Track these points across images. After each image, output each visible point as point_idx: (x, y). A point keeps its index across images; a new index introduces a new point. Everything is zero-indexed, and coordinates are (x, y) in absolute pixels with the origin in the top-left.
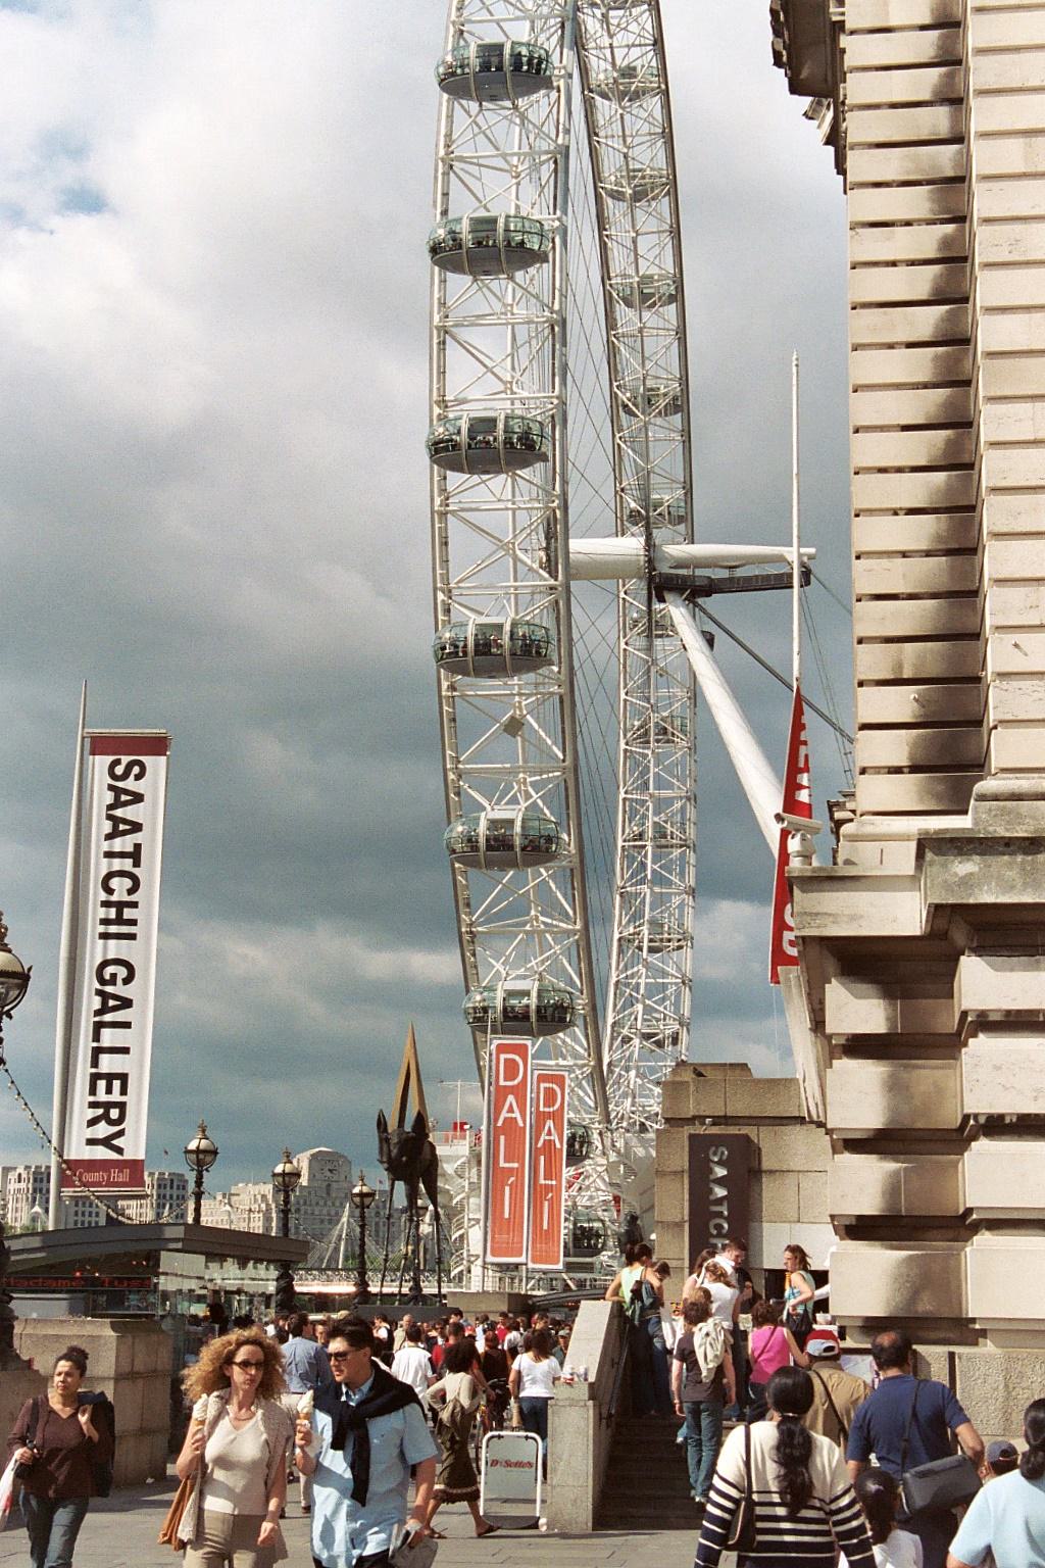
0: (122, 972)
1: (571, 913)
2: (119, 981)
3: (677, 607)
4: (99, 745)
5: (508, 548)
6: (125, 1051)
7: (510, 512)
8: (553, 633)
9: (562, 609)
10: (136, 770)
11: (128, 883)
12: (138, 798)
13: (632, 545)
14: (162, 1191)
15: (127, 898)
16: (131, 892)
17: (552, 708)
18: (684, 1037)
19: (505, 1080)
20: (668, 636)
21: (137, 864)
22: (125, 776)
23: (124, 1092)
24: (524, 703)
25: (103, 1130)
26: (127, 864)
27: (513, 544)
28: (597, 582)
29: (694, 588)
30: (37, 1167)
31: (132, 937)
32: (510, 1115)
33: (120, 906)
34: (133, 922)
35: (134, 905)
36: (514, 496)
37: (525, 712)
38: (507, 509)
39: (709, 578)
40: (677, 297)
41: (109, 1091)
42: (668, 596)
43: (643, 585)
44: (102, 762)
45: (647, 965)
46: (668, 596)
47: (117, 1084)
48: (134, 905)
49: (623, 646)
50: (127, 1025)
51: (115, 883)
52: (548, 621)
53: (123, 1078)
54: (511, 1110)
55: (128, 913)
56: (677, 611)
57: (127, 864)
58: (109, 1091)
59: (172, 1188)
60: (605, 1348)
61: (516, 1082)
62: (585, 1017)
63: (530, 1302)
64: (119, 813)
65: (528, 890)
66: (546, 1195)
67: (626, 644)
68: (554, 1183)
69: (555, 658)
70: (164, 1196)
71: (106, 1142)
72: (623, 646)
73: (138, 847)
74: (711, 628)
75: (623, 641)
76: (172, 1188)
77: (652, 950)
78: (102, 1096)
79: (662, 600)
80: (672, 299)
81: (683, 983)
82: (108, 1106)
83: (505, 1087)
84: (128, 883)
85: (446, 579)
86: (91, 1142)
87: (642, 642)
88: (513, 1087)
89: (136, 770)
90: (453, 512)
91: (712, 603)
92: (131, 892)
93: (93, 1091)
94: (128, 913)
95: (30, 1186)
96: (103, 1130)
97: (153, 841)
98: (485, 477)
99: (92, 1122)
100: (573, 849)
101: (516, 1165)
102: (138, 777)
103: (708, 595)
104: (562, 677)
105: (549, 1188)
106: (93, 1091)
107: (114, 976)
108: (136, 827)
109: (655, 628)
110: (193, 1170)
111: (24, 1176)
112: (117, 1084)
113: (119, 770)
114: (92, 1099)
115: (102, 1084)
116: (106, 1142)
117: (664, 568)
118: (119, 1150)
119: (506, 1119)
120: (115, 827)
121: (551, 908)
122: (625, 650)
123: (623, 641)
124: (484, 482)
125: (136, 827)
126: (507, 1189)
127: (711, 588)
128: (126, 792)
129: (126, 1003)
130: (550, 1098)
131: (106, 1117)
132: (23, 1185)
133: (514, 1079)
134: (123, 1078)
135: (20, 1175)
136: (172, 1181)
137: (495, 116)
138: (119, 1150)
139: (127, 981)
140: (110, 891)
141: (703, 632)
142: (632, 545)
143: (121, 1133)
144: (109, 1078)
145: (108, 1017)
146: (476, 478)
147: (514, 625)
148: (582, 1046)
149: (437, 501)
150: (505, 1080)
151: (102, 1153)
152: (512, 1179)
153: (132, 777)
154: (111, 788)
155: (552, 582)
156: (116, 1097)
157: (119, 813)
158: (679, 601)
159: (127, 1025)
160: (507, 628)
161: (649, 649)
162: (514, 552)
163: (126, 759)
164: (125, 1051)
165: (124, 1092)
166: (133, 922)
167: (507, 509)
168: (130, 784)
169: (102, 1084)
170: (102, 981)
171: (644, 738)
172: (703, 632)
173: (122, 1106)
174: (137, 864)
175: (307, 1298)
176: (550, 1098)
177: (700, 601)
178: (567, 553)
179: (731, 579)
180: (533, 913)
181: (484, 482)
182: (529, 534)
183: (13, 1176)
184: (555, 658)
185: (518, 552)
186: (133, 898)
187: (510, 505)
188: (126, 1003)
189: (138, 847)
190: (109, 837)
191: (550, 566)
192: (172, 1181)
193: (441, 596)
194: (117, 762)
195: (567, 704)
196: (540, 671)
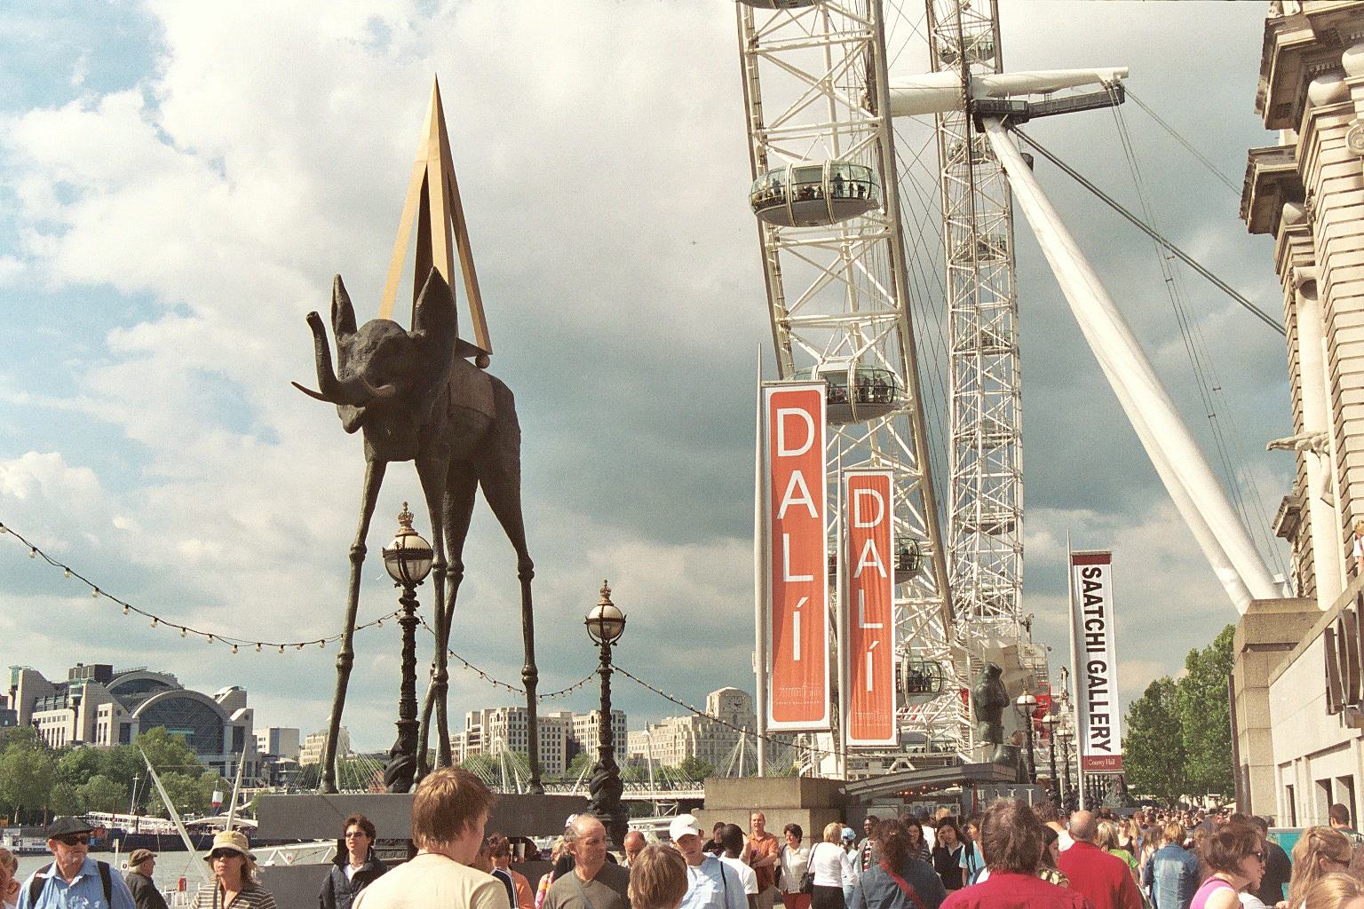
0: (1100, 667)
1: (913, 460)
2: (1100, 671)
3: (996, 132)
4: (1078, 559)
5: (827, 88)
6: (1106, 703)
7: (824, 47)
8: (876, 173)
9: (885, 146)
10: (1097, 573)
11: (1098, 625)
12: (1099, 586)
13: (950, 78)
14: (513, 722)
15: (1098, 632)
16: (1100, 629)
20: (984, 162)
21: (1101, 616)
22: (1091, 576)
23: (1107, 722)
24: (850, 248)
25: (1100, 740)
26: (1096, 616)
27: (830, 82)
28: (915, 117)
29: (1012, 118)
30: (511, 709)
31: (1103, 650)
32: (870, 564)
33: (1096, 636)
34: (1103, 643)
35: (1102, 635)
36: (827, 31)
37: (853, 257)
38: (819, 44)
39: (1026, 102)
41: (1100, 722)
42: (987, 124)
43: (963, 115)
44: (1081, 568)
46: (987, 124)
47: (1104, 719)
48: (1102, 635)
49: (944, 174)
50: (1105, 691)
51: (1091, 625)
52: (869, 160)
53: (1107, 716)
54: (797, 493)
55: (1100, 639)
56: (997, 139)
57: (1096, 616)
58: (1100, 722)
59: (520, 720)
62: (932, 559)
63: (842, 791)
64: (1088, 593)
65: (868, 438)
67: (947, 172)
68: (880, 626)
69: (880, 201)
70: (515, 726)
71: (1102, 746)
72: (944, 174)
73: (1101, 608)
75: (943, 171)
76: (520, 720)
78: (1097, 724)
81: (1016, 515)
82: (1100, 729)
84: (1098, 625)
85: (760, 126)
86: (1094, 746)
87: (962, 168)
89: (1097, 573)
90: (763, 53)
91: (1031, 127)
92: (1100, 629)
93: (1092, 723)
94: (1100, 639)
95: (506, 723)
96: (1100, 740)
97: (1108, 605)
98: (795, 12)
99: (1094, 736)
100: (910, 396)
101: (809, 578)
102: (1098, 576)
104: (890, 220)
106: (1092, 723)
107: (1096, 669)
108: (1100, 600)
109: (974, 155)
111: (502, 715)
112: (1104, 719)
113: (1088, 573)
114: (1092, 726)
115: (1096, 720)
116: (1102, 746)
117: (981, 96)
118: (1109, 750)
120: (1089, 600)
121: (890, 449)
122: (946, 178)
123: (943, 171)
124: (794, 19)
125: (1100, 600)
127: (1027, 114)
128: (1093, 583)
129: (1104, 681)
131: (1100, 734)
132: (501, 723)
134: (1107, 716)
135: (593, 717)
136: (520, 714)
138: (1109, 750)
139: (1103, 671)
140: (1091, 629)
141: (1022, 154)
142: (950, 78)
143: (1108, 742)
144: (1100, 716)
145: (1094, 688)
146: (785, 15)
148: (931, 583)
149: (746, 43)
151: (1103, 752)
152: (804, 600)
153: (1090, 570)
154: (1084, 582)
155: (871, 118)
156: (1104, 725)
157: (1088, 593)
158: (998, 126)
159: (1105, 691)
161: (970, 176)
162: (831, 90)
163: (1091, 567)
164: (1106, 703)
165: (1107, 722)
166: (1103, 643)
167: (819, 44)
168: (1094, 579)
169: (1096, 720)
170: (1091, 671)
172: (1022, 154)
173: (1107, 729)
174: (1101, 616)
178: (886, 88)
179: (1046, 103)
180: (873, 455)
181: (794, 19)
182: (845, 70)
183: (493, 716)
184: (880, 201)
185: (835, 90)
186: (1101, 632)
187: (822, 40)
188: (1104, 681)
189: (1101, 608)
190: (1086, 605)
191: (871, 101)
192: (520, 714)
193: (756, 143)
194: (1087, 569)
195: (896, 242)
196: (865, 214)
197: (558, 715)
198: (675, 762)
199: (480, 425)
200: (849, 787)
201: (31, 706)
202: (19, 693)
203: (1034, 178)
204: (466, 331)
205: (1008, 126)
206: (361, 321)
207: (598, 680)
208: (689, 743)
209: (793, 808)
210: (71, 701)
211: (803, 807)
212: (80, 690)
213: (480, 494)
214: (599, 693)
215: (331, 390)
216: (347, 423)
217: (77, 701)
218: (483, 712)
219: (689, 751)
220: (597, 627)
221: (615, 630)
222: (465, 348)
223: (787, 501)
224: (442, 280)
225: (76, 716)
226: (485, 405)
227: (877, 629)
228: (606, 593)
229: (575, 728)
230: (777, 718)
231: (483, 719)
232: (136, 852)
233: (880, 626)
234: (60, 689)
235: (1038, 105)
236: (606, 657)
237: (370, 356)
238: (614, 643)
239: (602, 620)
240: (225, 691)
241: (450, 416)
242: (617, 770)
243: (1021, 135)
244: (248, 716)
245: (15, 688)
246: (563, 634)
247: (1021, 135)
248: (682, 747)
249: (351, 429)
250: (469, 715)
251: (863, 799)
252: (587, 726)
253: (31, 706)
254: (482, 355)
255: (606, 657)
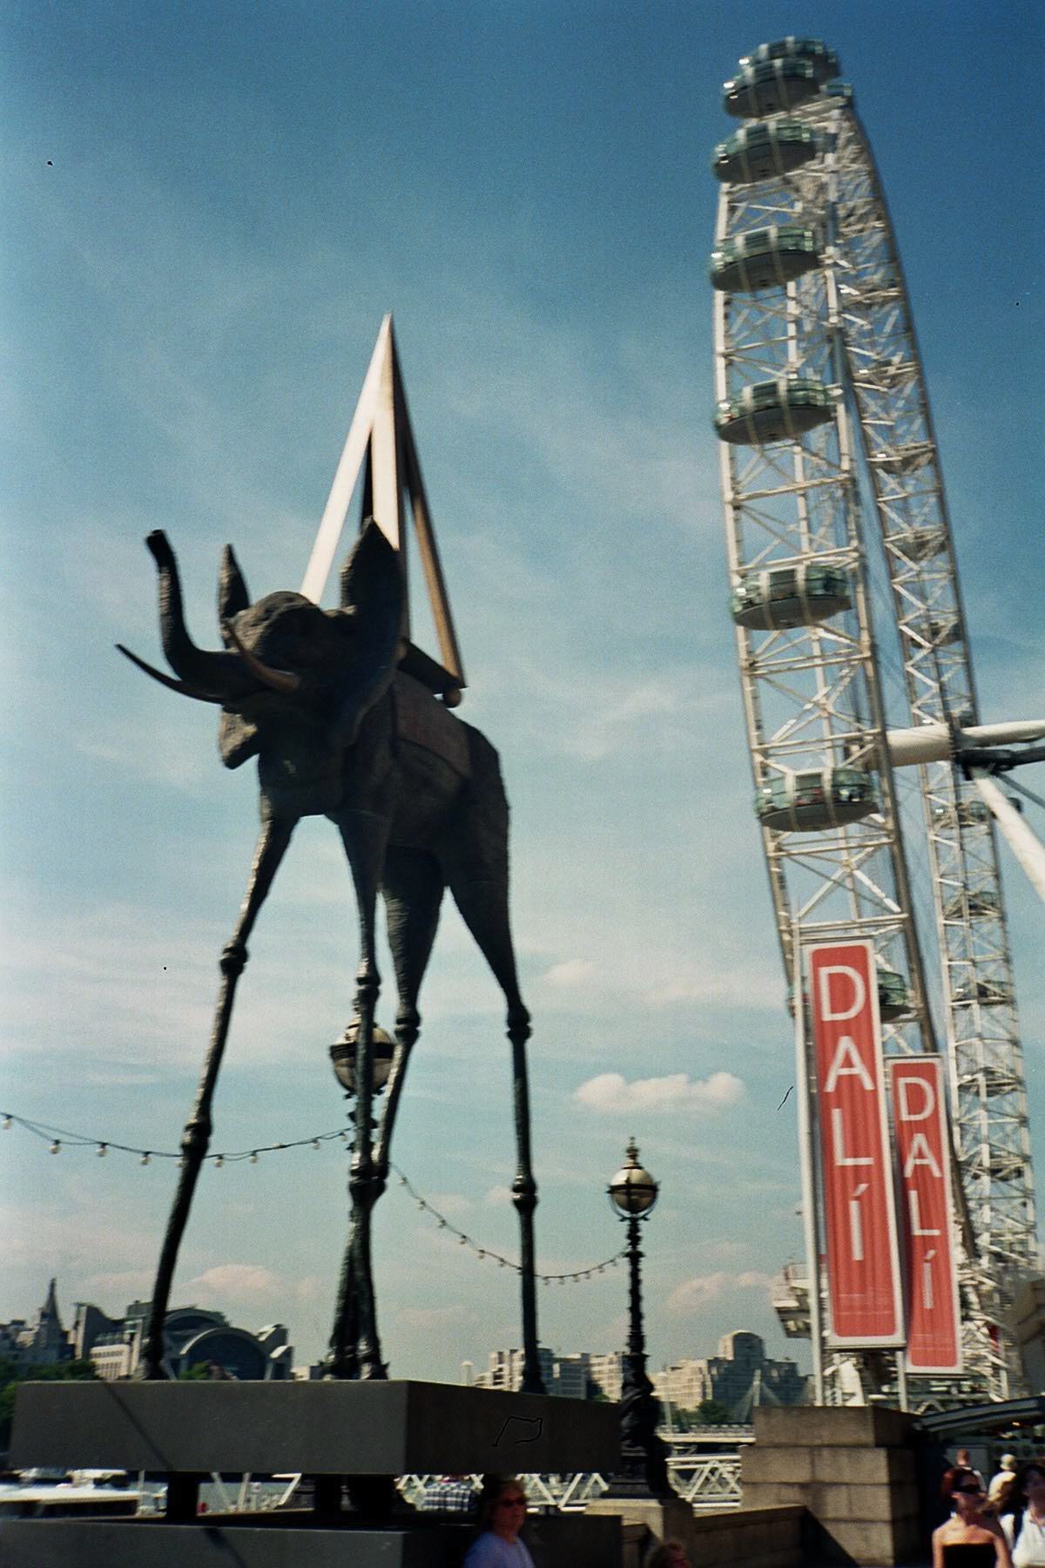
17: (882, 861)
18: (1027, 1169)
19: (834, 1010)
40: (946, 545)
42: (975, 772)
45: (985, 1106)
54: (848, 1063)
60: (504, 837)
61: (852, 1013)
63: (918, 1427)
66: (925, 1252)
68: (936, 1232)
74: (1017, 795)
77: (989, 1094)
79: (969, 777)
80: (942, 547)
83: (833, 1023)
88: (847, 1022)
91: (1019, 773)
103: (1010, 768)
105: (928, 1242)
110: (624, 1219)
119: (840, 1078)
126: (854, 1206)
127: (1015, 760)
130: (916, 1099)
133: (846, 1009)
137: (789, 452)
147: (835, 773)
150: (834, 1010)
152: (863, 1187)
160: (827, 777)
171: (958, 913)
175: (948, 1340)
176: (916, 1099)
177: (1008, 773)
179: (1032, 751)
197: (577, 1356)
198: (691, 1404)
199: (447, 782)
200: (927, 1422)
201: (90, 1342)
202: (81, 1329)
203: (1026, 822)
204: (424, 634)
205: (996, 772)
206: (258, 592)
207: (625, 1265)
208: (704, 1386)
209: (864, 1446)
210: (127, 1337)
211: (878, 1445)
212: (134, 1327)
213: (448, 895)
214: (626, 1283)
215: (191, 671)
216: (226, 751)
217: (132, 1335)
218: (507, 1353)
219: (704, 1394)
220: (623, 1198)
221: (645, 1200)
222: (417, 660)
223: (836, 1071)
224: (385, 542)
225: (131, 1352)
226: (456, 752)
227: (932, 1237)
228: (633, 1153)
229: (595, 1369)
230: (840, 1331)
231: (506, 1359)
232: (676, 1488)
233: (936, 1232)
234: (117, 1325)
235: (1023, 753)
236: (634, 1237)
237: (259, 630)
238: (644, 1218)
239: (628, 1186)
240: (269, 1329)
241: (395, 752)
242: (651, 1387)
243: (1009, 782)
244: (288, 1354)
245: (77, 1323)
246: (575, 1181)
247: (1009, 782)
248: (698, 1390)
249: (234, 760)
250: (494, 1355)
251: (941, 1437)
252: (606, 1368)
253: (90, 1342)
254: (451, 684)
255: (634, 1237)
